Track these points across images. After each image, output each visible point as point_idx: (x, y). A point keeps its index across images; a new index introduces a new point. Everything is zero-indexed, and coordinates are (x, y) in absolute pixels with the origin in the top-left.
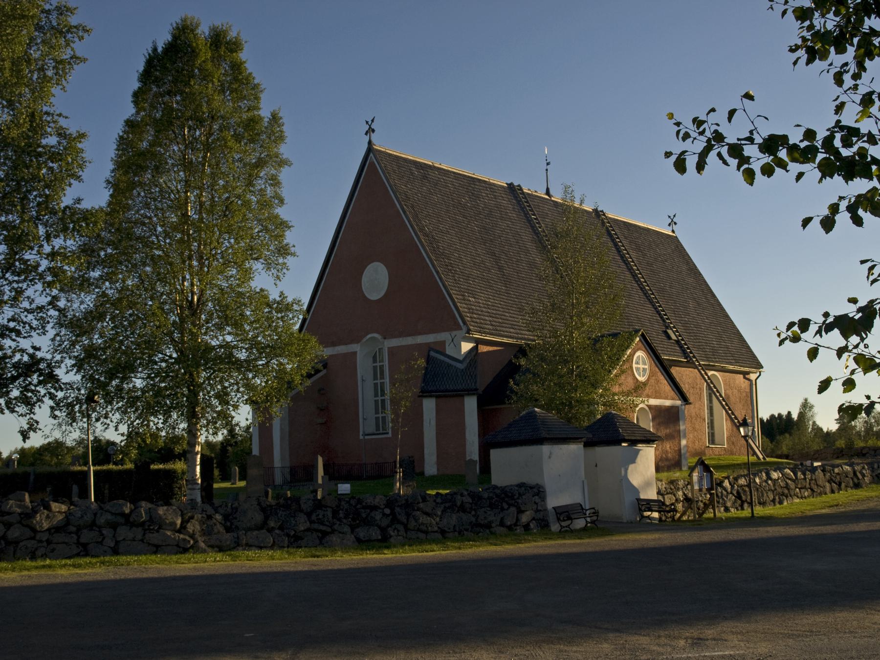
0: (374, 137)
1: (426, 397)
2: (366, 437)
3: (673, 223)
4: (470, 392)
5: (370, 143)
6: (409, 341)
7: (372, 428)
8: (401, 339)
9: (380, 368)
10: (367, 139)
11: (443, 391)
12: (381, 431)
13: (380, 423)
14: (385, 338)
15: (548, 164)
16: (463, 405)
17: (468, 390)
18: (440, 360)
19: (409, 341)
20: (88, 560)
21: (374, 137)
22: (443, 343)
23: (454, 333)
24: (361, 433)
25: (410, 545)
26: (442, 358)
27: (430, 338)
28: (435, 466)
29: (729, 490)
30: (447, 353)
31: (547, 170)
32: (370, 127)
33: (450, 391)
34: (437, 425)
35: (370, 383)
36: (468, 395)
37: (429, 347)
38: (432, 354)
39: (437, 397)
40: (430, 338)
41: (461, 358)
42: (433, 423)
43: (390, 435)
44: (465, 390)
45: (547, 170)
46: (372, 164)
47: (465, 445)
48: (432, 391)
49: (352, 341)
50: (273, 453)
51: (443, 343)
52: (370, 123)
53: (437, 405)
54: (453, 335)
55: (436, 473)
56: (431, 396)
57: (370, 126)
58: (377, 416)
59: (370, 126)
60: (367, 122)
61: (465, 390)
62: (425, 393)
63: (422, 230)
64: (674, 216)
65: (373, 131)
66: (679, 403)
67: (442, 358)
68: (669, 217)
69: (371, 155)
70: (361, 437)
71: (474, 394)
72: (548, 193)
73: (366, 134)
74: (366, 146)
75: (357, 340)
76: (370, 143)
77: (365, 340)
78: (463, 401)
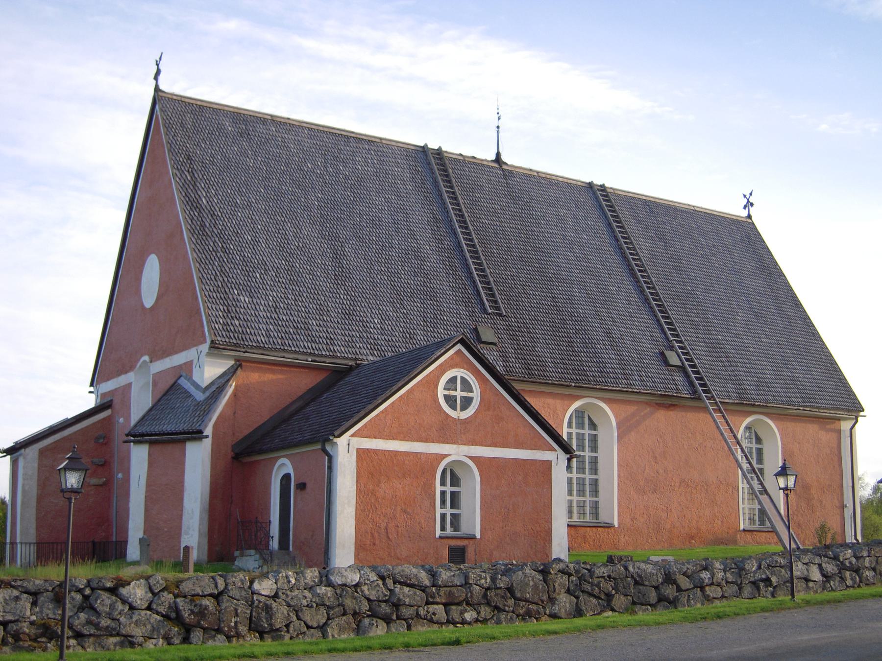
3: (749, 204)
9: (584, 468)
16: (184, 454)
25: (19, 651)
29: (427, 582)
31: (498, 127)
32: (748, 201)
34: (148, 485)
39: (151, 443)
42: (143, 481)
45: (498, 127)
47: (180, 517)
52: (748, 197)
53: (150, 455)
57: (748, 200)
58: (455, 511)
59: (748, 200)
60: (745, 196)
65: (752, 205)
68: (745, 196)
73: (745, 208)
78: (184, 449)
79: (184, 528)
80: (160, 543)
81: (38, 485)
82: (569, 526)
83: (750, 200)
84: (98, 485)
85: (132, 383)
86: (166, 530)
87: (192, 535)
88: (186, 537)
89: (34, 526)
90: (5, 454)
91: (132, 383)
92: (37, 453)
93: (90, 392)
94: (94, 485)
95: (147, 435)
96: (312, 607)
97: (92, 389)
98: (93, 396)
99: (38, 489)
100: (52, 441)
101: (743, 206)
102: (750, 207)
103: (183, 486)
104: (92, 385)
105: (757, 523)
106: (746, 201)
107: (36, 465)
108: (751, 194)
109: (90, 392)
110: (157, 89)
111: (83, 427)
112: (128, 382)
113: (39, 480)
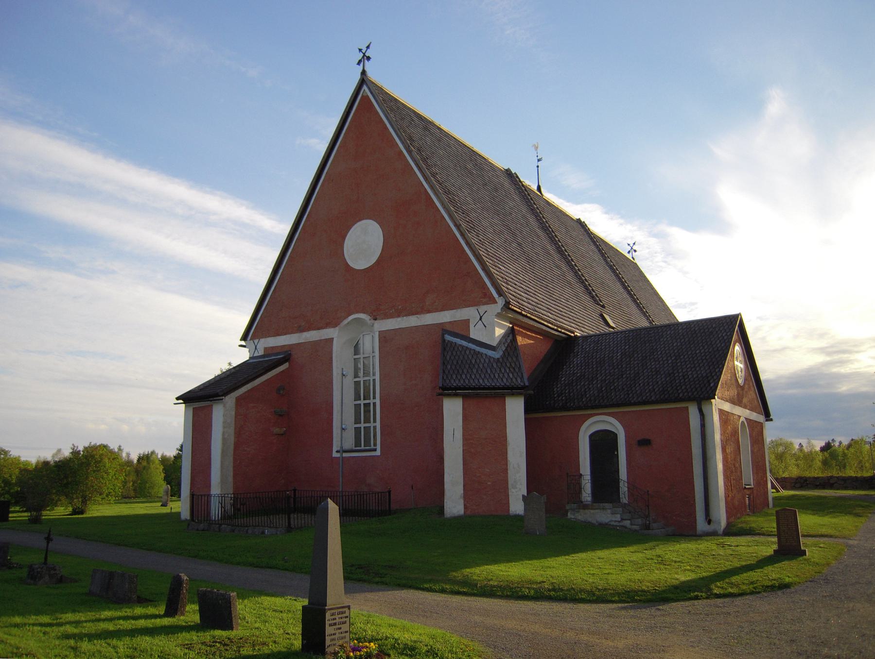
0: (369, 66)
1: (449, 395)
2: (345, 455)
4: (514, 390)
5: (364, 73)
6: (413, 321)
7: (349, 443)
8: (399, 319)
10: (360, 68)
11: (474, 389)
12: (363, 447)
13: (362, 437)
14: (375, 319)
15: (539, 160)
16: (504, 410)
17: (512, 388)
18: (462, 347)
19: (413, 321)
20: (142, 500)
21: (369, 66)
22: (467, 322)
23: (482, 309)
24: (335, 449)
26: (464, 343)
27: (445, 317)
28: (462, 501)
30: (471, 336)
31: (538, 167)
33: (484, 389)
35: (349, 381)
36: (513, 395)
37: (444, 329)
38: (448, 338)
39: (465, 397)
40: (445, 317)
41: (494, 344)
43: (378, 453)
44: (508, 388)
45: (538, 167)
46: (365, 98)
47: (506, 471)
48: (456, 388)
49: (327, 325)
50: (210, 474)
51: (467, 322)
52: (364, 51)
54: (482, 311)
55: (462, 512)
56: (456, 395)
57: (364, 54)
59: (364, 54)
60: (360, 50)
61: (508, 388)
62: (448, 390)
63: (434, 175)
64: (634, 244)
65: (369, 58)
66: (761, 418)
67: (464, 343)
69: (365, 87)
70: (335, 455)
71: (519, 394)
72: (539, 188)
73: (359, 63)
74: (358, 77)
75: (333, 323)
76: (364, 73)
77: (346, 322)
79: (510, 482)
80: (485, 497)
81: (235, 433)
82: (112, 575)
83: (366, 54)
84: (279, 434)
85: (333, 338)
86: (489, 483)
87: (520, 489)
88: (513, 490)
89: (232, 474)
90: (181, 401)
91: (333, 338)
92: (234, 400)
93: (241, 346)
94: (276, 434)
95: (460, 389)
96: (288, 611)
97: (243, 343)
98: (246, 350)
99: (235, 438)
100: (246, 390)
101: (357, 61)
102: (366, 61)
103: (506, 440)
104: (244, 338)
105: (330, 622)
106: (362, 55)
107: (234, 413)
108: (368, 47)
109: (241, 346)
110: (364, 80)
111: (269, 377)
112: (330, 337)
113: (235, 429)
